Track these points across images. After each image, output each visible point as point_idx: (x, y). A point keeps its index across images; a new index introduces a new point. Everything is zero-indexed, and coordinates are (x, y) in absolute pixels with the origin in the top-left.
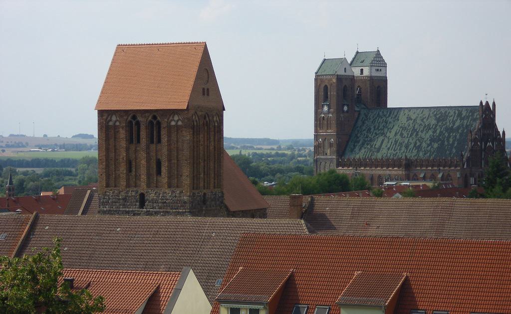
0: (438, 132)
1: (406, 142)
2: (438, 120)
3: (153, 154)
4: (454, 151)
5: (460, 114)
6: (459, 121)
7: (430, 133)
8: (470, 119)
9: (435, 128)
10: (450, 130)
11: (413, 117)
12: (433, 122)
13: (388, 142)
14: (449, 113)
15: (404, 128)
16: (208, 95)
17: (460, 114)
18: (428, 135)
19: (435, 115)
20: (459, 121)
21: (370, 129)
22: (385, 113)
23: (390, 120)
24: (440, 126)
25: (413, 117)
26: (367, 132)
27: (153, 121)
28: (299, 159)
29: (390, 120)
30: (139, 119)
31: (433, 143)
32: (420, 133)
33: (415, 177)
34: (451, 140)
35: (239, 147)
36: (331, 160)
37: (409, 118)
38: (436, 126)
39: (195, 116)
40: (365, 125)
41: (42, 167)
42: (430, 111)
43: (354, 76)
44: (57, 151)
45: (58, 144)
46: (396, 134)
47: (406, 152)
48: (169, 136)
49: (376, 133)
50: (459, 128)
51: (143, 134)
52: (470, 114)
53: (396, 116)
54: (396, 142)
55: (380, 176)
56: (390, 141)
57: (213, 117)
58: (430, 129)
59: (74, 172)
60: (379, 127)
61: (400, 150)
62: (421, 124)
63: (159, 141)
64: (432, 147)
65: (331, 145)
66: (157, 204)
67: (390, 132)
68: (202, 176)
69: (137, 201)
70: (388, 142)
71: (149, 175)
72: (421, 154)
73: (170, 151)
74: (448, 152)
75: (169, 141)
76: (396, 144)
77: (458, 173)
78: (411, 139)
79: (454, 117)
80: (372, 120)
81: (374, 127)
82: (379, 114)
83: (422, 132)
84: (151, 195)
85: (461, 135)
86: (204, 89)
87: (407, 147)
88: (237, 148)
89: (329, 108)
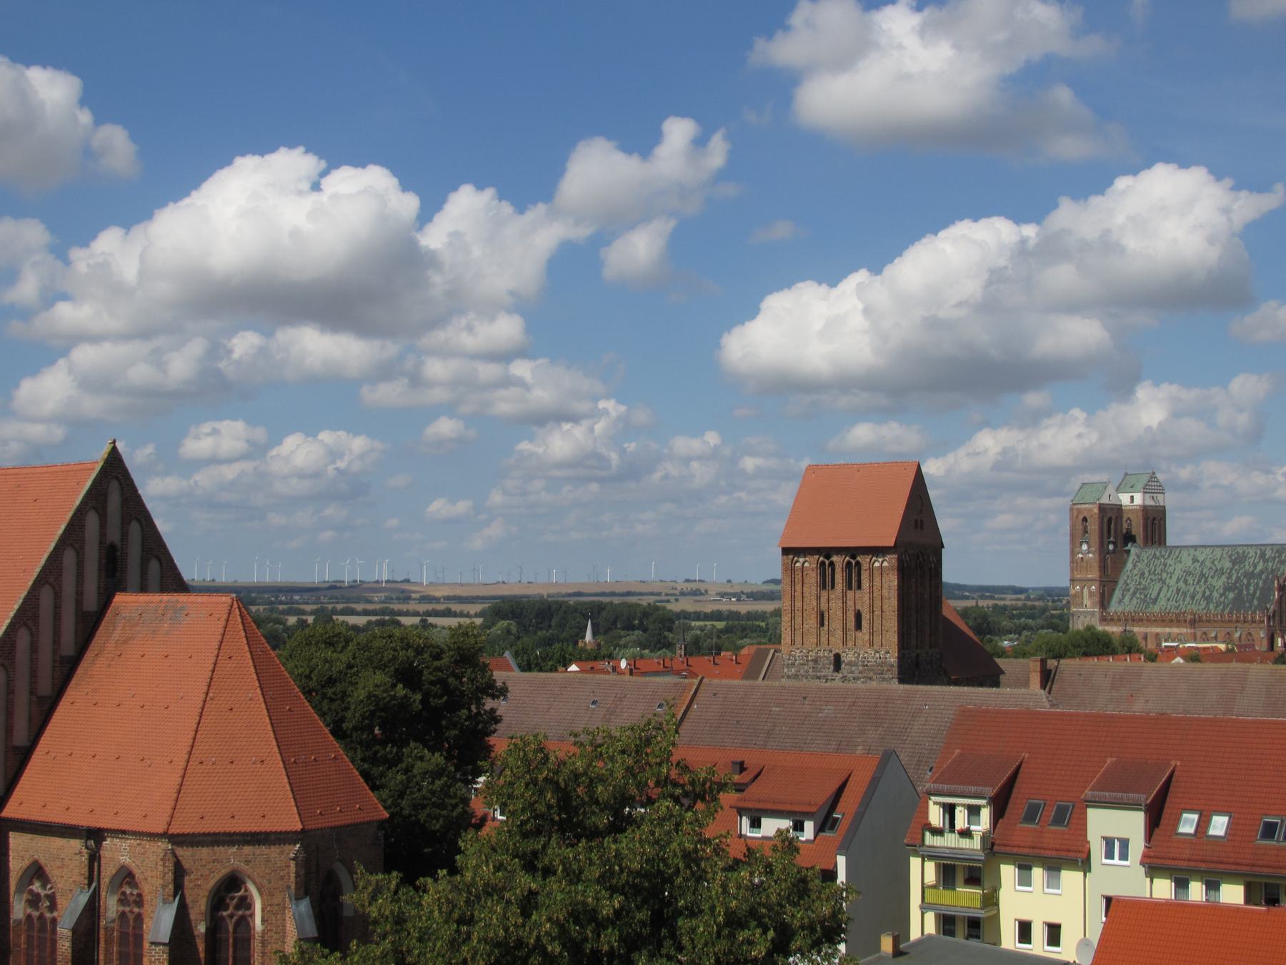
0: (1234, 577)
1: (1192, 590)
2: (1234, 563)
3: (850, 603)
4: (1256, 602)
5: (1263, 555)
6: (1261, 564)
7: (1224, 578)
8: (1276, 562)
9: (1230, 572)
10: (1250, 576)
11: (1201, 558)
12: (1227, 564)
13: (1168, 591)
14: (1249, 553)
15: (1188, 573)
16: (922, 528)
17: (1263, 555)
18: (1220, 583)
19: (1230, 557)
20: (1261, 564)
21: (1143, 574)
22: (1163, 553)
23: (1170, 561)
24: (1236, 570)
25: (1201, 558)
26: (1140, 578)
27: (852, 560)
28: (1054, 612)
29: (1170, 561)
30: (835, 558)
31: (1227, 593)
32: (1210, 579)
33: (1204, 636)
34: (1252, 588)
35: (975, 596)
36: (1093, 614)
37: (1195, 560)
38: (1231, 570)
39: (905, 555)
40: (1137, 568)
41: (724, 620)
42: (1223, 550)
43: (1121, 506)
44: (744, 600)
45: (745, 591)
46: (1178, 580)
47: (1192, 604)
48: (871, 580)
49: (1151, 579)
50: (1262, 572)
51: (839, 578)
52: (1277, 555)
53: (1178, 557)
54: (1178, 590)
55: (1157, 634)
56: (1171, 589)
57: (929, 557)
58: (1223, 573)
59: (764, 626)
60: (1155, 570)
61: (1184, 600)
62: (1211, 568)
63: (859, 587)
64: (1226, 598)
65: (1091, 594)
66: (856, 668)
67: (1171, 578)
68: (914, 632)
69: (830, 664)
70: (1168, 591)
71: (845, 630)
72: (1212, 607)
73: (872, 599)
74: (1247, 604)
75: (871, 587)
76: (1178, 594)
77: (1261, 632)
78: (1198, 587)
79: (1255, 558)
80: (1146, 562)
81: (1149, 571)
82: (1155, 554)
83: (1213, 577)
84: (848, 656)
85: (1265, 582)
86: (916, 521)
87: (1193, 597)
88: (973, 598)
89: (1089, 547)
